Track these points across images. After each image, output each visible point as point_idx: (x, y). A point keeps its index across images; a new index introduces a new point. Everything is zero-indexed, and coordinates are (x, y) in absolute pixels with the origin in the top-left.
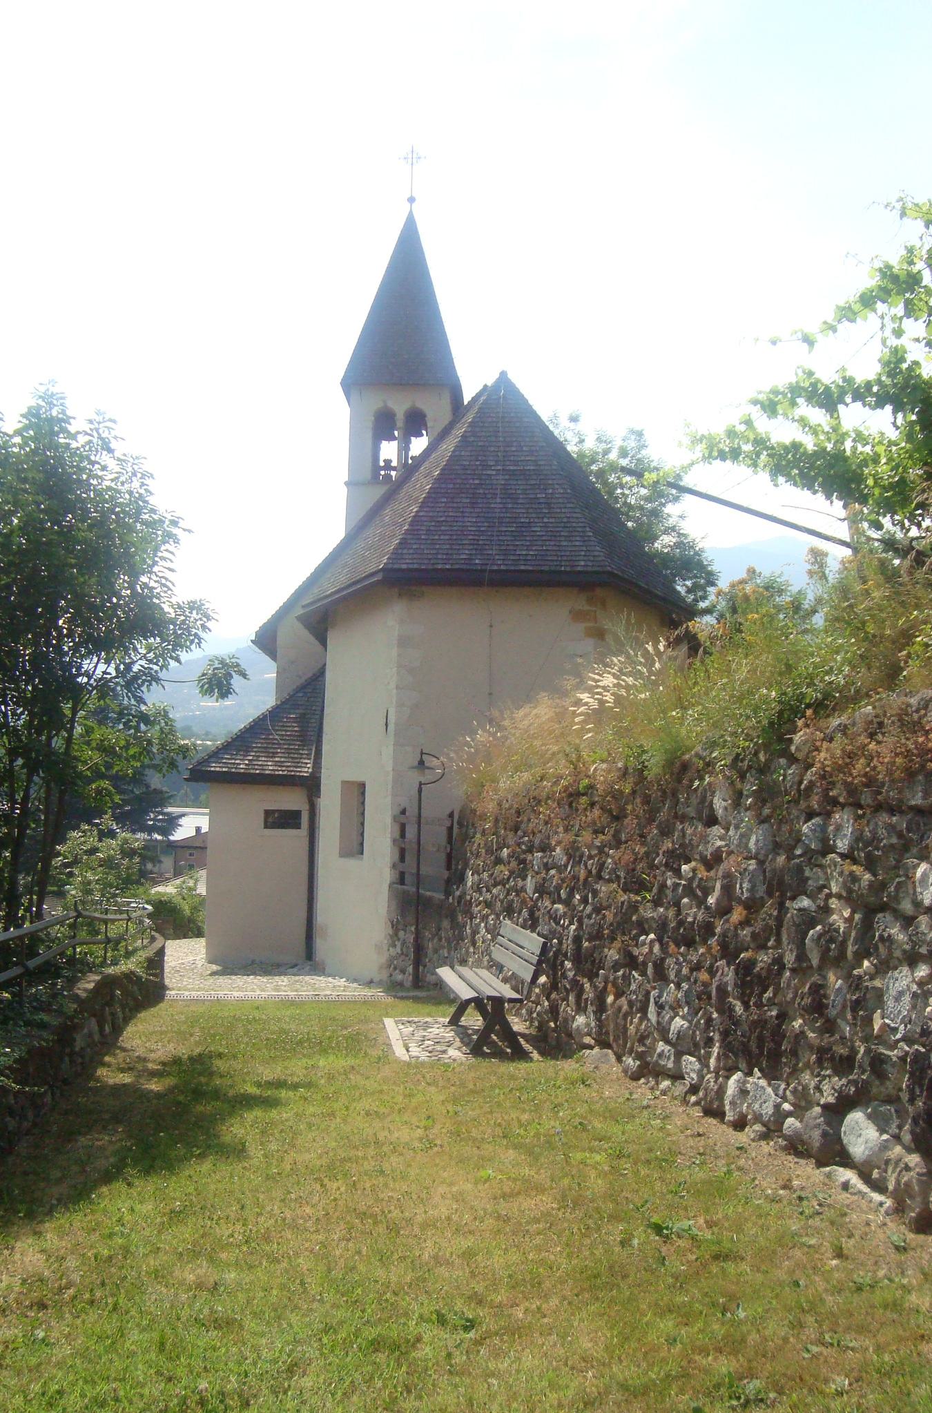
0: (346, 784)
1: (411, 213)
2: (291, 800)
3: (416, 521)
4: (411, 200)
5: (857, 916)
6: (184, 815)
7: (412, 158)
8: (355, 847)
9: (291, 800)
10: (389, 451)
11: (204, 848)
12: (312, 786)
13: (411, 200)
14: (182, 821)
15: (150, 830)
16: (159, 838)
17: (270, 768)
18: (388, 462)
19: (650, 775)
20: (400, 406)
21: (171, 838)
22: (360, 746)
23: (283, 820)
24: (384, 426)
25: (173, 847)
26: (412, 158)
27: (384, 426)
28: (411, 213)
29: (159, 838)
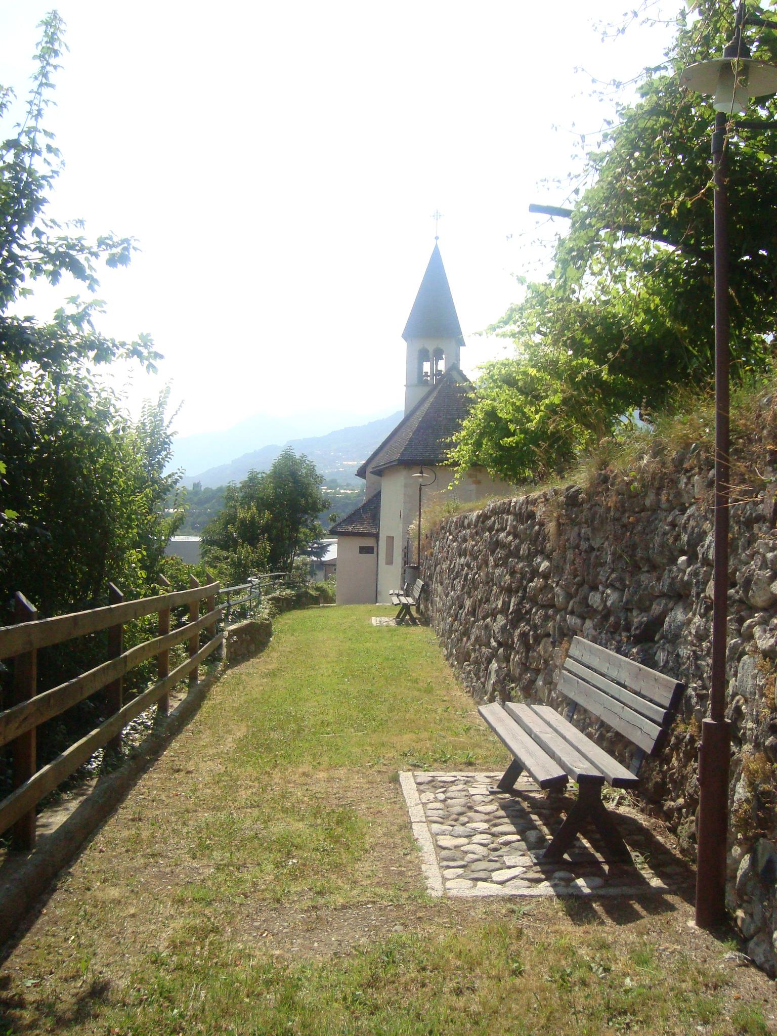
0: (388, 537)
1: (436, 248)
2: (368, 542)
3: (411, 440)
4: (437, 238)
5: (303, 501)
6: (329, 545)
7: (437, 216)
8: (390, 562)
9: (368, 542)
10: (427, 367)
11: (335, 565)
12: (376, 536)
13: (437, 238)
14: (329, 548)
15: (309, 554)
16: (315, 559)
17: (361, 529)
18: (426, 373)
19: (179, 485)
20: (431, 347)
21: (323, 559)
22: (392, 523)
23: (365, 550)
24: (424, 355)
25: (323, 564)
26: (437, 216)
27: (424, 355)
28: (436, 248)
29: (315, 559)
